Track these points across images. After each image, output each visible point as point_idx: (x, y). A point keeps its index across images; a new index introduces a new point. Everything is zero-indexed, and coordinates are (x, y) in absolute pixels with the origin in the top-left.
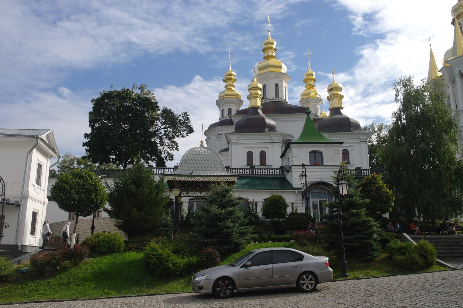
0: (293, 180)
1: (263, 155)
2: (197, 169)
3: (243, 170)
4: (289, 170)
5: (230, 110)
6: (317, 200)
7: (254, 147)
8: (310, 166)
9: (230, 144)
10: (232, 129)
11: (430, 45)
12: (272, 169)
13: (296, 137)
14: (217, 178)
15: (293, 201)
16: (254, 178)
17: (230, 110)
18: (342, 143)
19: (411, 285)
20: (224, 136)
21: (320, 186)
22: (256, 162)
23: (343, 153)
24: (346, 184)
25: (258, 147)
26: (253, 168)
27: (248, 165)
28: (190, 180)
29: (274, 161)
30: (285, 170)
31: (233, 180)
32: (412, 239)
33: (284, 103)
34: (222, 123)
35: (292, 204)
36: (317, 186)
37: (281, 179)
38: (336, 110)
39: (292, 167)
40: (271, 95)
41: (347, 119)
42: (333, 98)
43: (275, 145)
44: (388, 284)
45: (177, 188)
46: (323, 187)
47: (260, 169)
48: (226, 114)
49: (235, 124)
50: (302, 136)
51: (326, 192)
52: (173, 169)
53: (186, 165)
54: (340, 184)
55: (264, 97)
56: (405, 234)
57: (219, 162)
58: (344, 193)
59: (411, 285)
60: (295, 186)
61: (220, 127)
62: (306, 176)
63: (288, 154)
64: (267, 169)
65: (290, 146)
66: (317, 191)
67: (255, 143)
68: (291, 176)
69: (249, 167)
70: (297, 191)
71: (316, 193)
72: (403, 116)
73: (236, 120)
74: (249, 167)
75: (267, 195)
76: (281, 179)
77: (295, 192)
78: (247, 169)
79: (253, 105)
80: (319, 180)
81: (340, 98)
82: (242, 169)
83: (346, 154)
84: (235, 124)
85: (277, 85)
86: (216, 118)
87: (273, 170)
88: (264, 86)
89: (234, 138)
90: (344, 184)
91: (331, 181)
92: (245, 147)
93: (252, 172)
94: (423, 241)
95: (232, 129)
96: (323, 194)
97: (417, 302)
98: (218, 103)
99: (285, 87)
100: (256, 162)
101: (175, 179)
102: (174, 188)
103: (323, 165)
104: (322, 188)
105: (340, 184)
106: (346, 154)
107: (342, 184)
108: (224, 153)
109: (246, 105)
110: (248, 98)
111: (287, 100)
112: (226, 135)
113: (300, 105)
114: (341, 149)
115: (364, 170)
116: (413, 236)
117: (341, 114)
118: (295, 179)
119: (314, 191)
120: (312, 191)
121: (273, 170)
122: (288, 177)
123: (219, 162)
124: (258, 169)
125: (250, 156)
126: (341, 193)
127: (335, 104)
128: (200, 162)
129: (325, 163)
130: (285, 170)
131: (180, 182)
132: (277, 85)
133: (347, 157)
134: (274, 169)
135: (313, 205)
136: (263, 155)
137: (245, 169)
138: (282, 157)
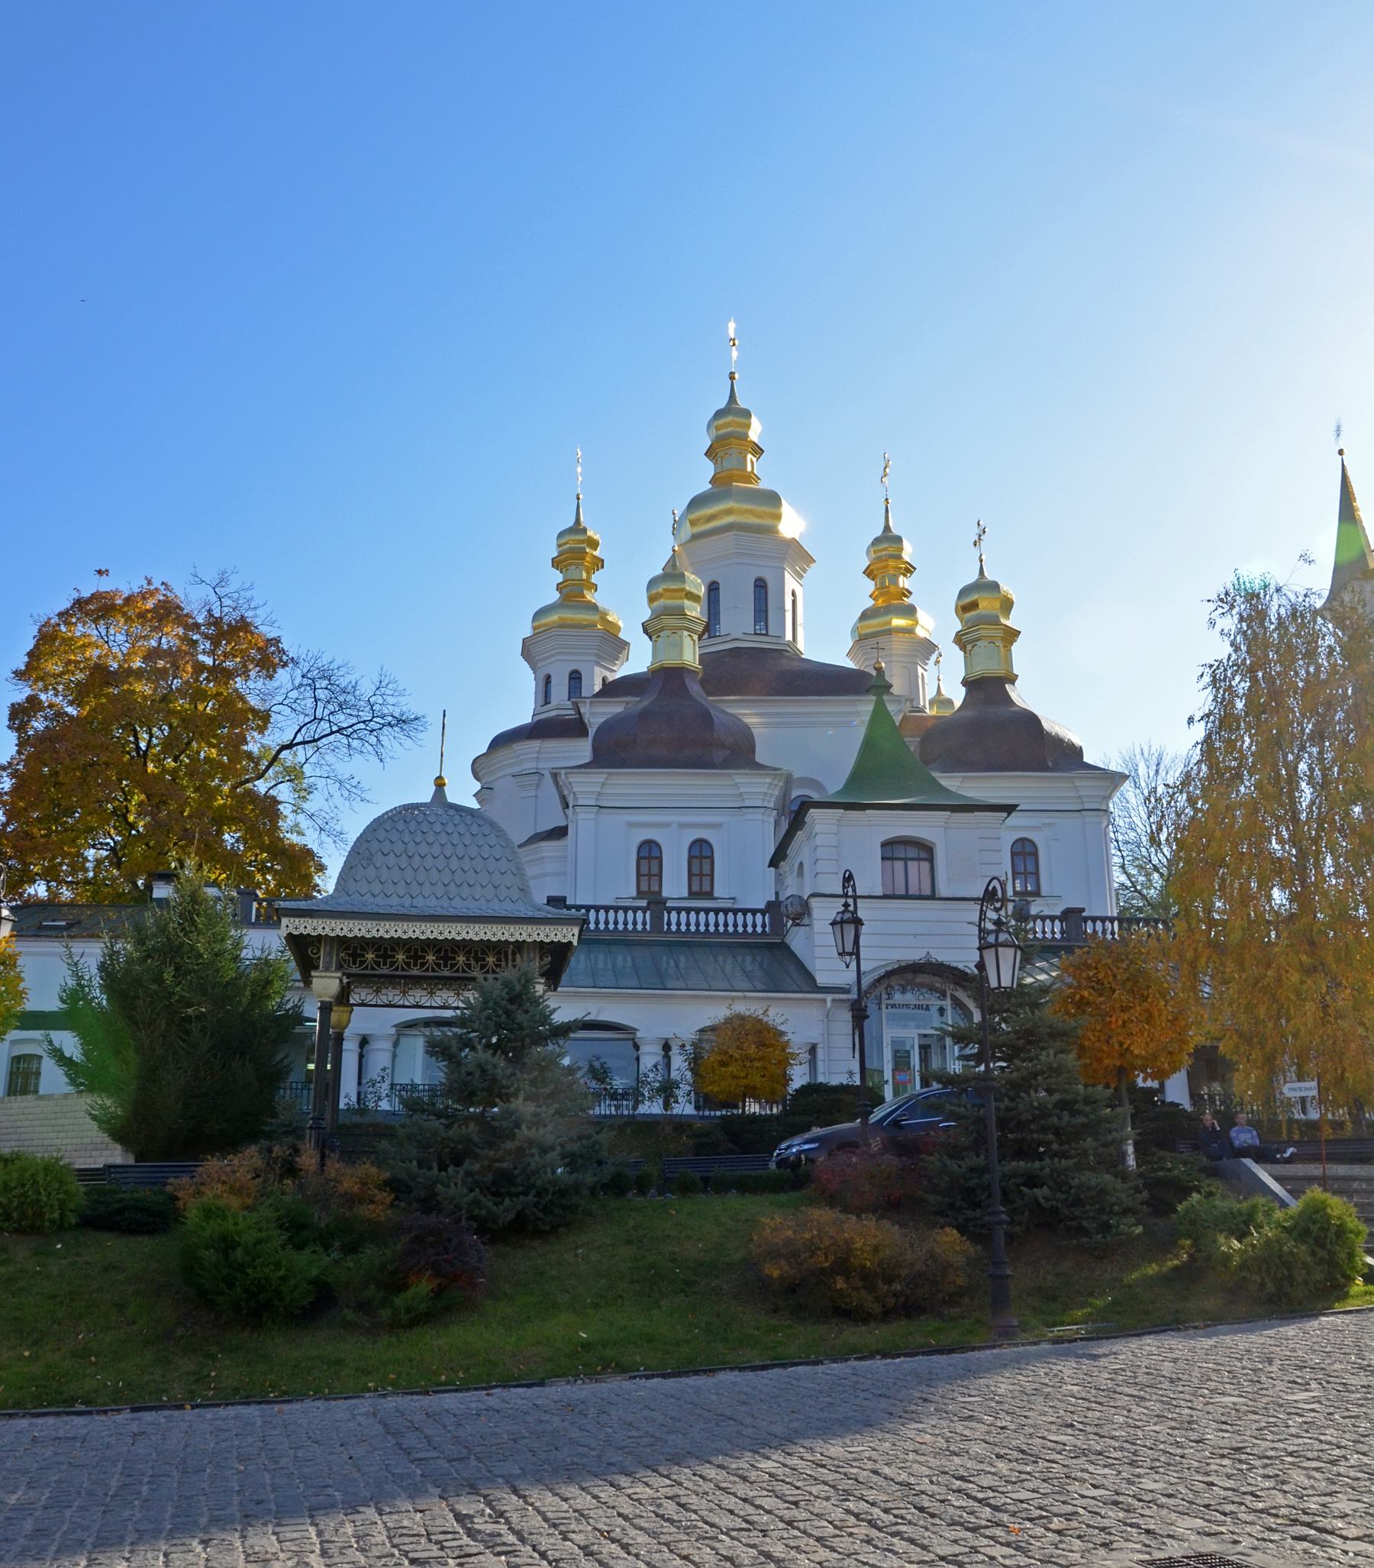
0: (818, 952)
1: (701, 853)
2: (415, 889)
3: (621, 914)
4: (802, 913)
5: (575, 677)
6: (911, 1035)
7: (667, 825)
8: (885, 897)
9: (569, 812)
10: (582, 750)
11: (1341, 452)
12: (735, 912)
13: (834, 785)
14: (495, 928)
15: (813, 1035)
16: (658, 944)
17: (575, 677)
18: (1009, 809)
19: (1270, 1361)
20: (548, 777)
21: (922, 978)
22: (675, 885)
23: (1014, 854)
24: (1013, 946)
25: (683, 826)
26: (657, 904)
27: (640, 894)
28: (382, 933)
29: (745, 882)
30: (784, 913)
31: (559, 938)
32: (1276, 1178)
33: (786, 653)
34: (539, 730)
35: (813, 1049)
36: (910, 976)
37: (768, 950)
38: (988, 688)
39: (815, 903)
40: (738, 625)
41: (1031, 721)
42: (979, 639)
43: (750, 815)
44: (1175, 1361)
45: (327, 969)
46: (938, 982)
47: (688, 910)
48: (560, 691)
49: (592, 731)
50: (857, 779)
51: (947, 1003)
52: (763, 912)
53: (371, 872)
54: (991, 946)
55: (710, 629)
56: (1248, 1162)
57: (504, 865)
58: (1006, 982)
59: (1270, 1361)
60: (822, 979)
61: (535, 744)
62: (858, 922)
63: (801, 849)
64: (717, 911)
65: (807, 819)
66: (909, 998)
67: (669, 804)
68: (809, 939)
69: (643, 903)
70: (829, 998)
71: (907, 1006)
72: (1242, 685)
73: (596, 715)
74: (643, 903)
75: (713, 1011)
76: (768, 950)
77: (825, 1000)
78: (635, 910)
79: (670, 661)
80: (916, 955)
81: (1003, 639)
82: (616, 909)
83: (1024, 852)
84: (592, 731)
85: (761, 585)
86: (520, 708)
87: (740, 916)
88: (713, 588)
89: (587, 786)
90: (1005, 945)
91: (965, 958)
92: (631, 825)
93: (657, 920)
94: (1316, 1193)
95: (582, 750)
96: (934, 1010)
97: (1293, 1430)
98: (528, 651)
99: (794, 594)
100: (675, 885)
101: (320, 931)
102: (316, 968)
103: (932, 897)
104: (932, 989)
105: (991, 946)
106: (1024, 852)
107: (996, 945)
108: (549, 847)
109: (639, 659)
110: (646, 631)
111: (801, 645)
112: (555, 776)
113: (850, 664)
114: (1009, 838)
115: (1094, 920)
116: (1280, 1169)
117: (1009, 701)
118: (817, 945)
119: (898, 998)
120: (890, 996)
121: (740, 916)
122: (796, 939)
123: (504, 865)
124: (679, 910)
125: (649, 854)
126: (994, 984)
127: (987, 666)
128: (429, 862)
129: (943, 890)
130: (784, 913)
131: (342, 942)
132: (761, 585)
133: (1031, 868)
134: (745, 912)
135: (896, 1052)
136: (701, 853)
137: (626, 909)
138: (774, 862)
